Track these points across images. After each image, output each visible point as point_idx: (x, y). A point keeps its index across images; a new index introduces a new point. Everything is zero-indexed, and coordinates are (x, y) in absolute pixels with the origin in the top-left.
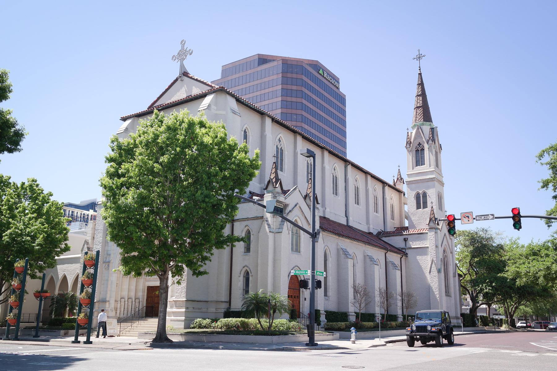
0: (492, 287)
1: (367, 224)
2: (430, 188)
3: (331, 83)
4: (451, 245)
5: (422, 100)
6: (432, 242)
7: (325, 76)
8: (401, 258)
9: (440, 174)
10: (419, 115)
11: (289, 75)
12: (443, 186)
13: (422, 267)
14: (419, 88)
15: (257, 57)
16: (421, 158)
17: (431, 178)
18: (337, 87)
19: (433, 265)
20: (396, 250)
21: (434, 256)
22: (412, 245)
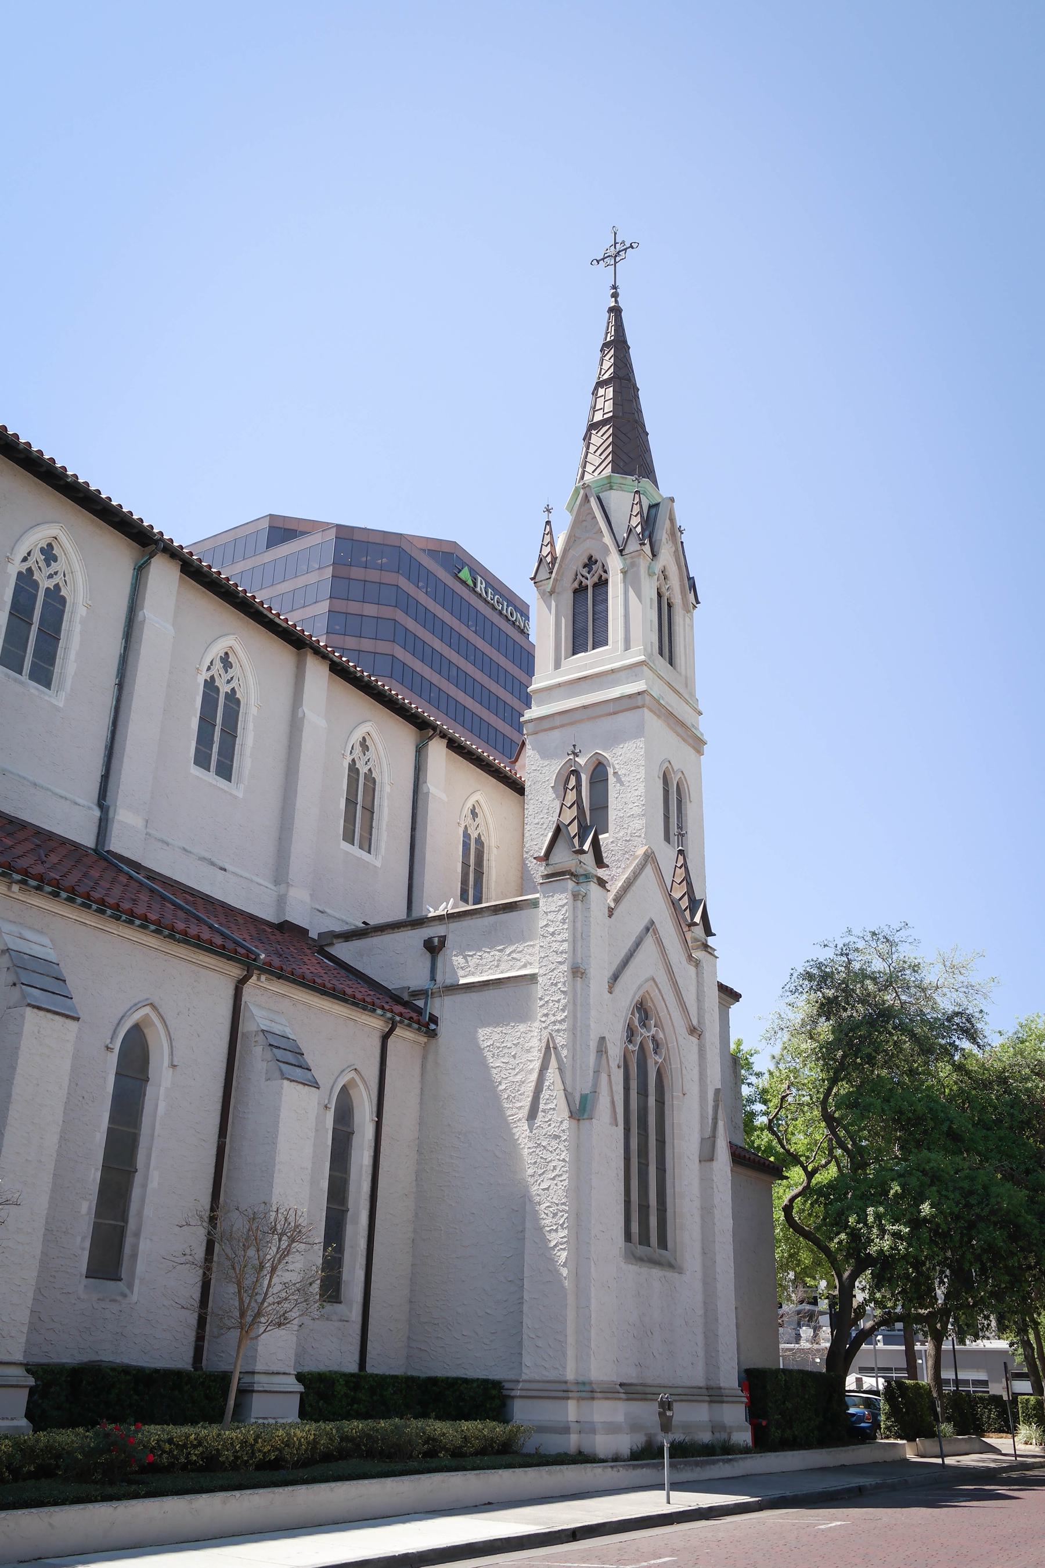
0: (916, 1223)
1: (277, 882)
2: (624, 741)
3: (500, 613)
4: (693, 989)
5: (614, 398)
6: (555, 945)
7: (478, 589)
8: (385, 1038)
9: (685, 692)
10: (599, 452)
11: (357, 573)
12: (699, 752)
13: (501, 1088)
14: (607, 358)
15: (266, 525)
16: (594, 620)
17: (630, 696)
18: (519, 627)
19: (552, 1074)
20: (370, 996)
21: (560, 1022)
22: (461, 973)
